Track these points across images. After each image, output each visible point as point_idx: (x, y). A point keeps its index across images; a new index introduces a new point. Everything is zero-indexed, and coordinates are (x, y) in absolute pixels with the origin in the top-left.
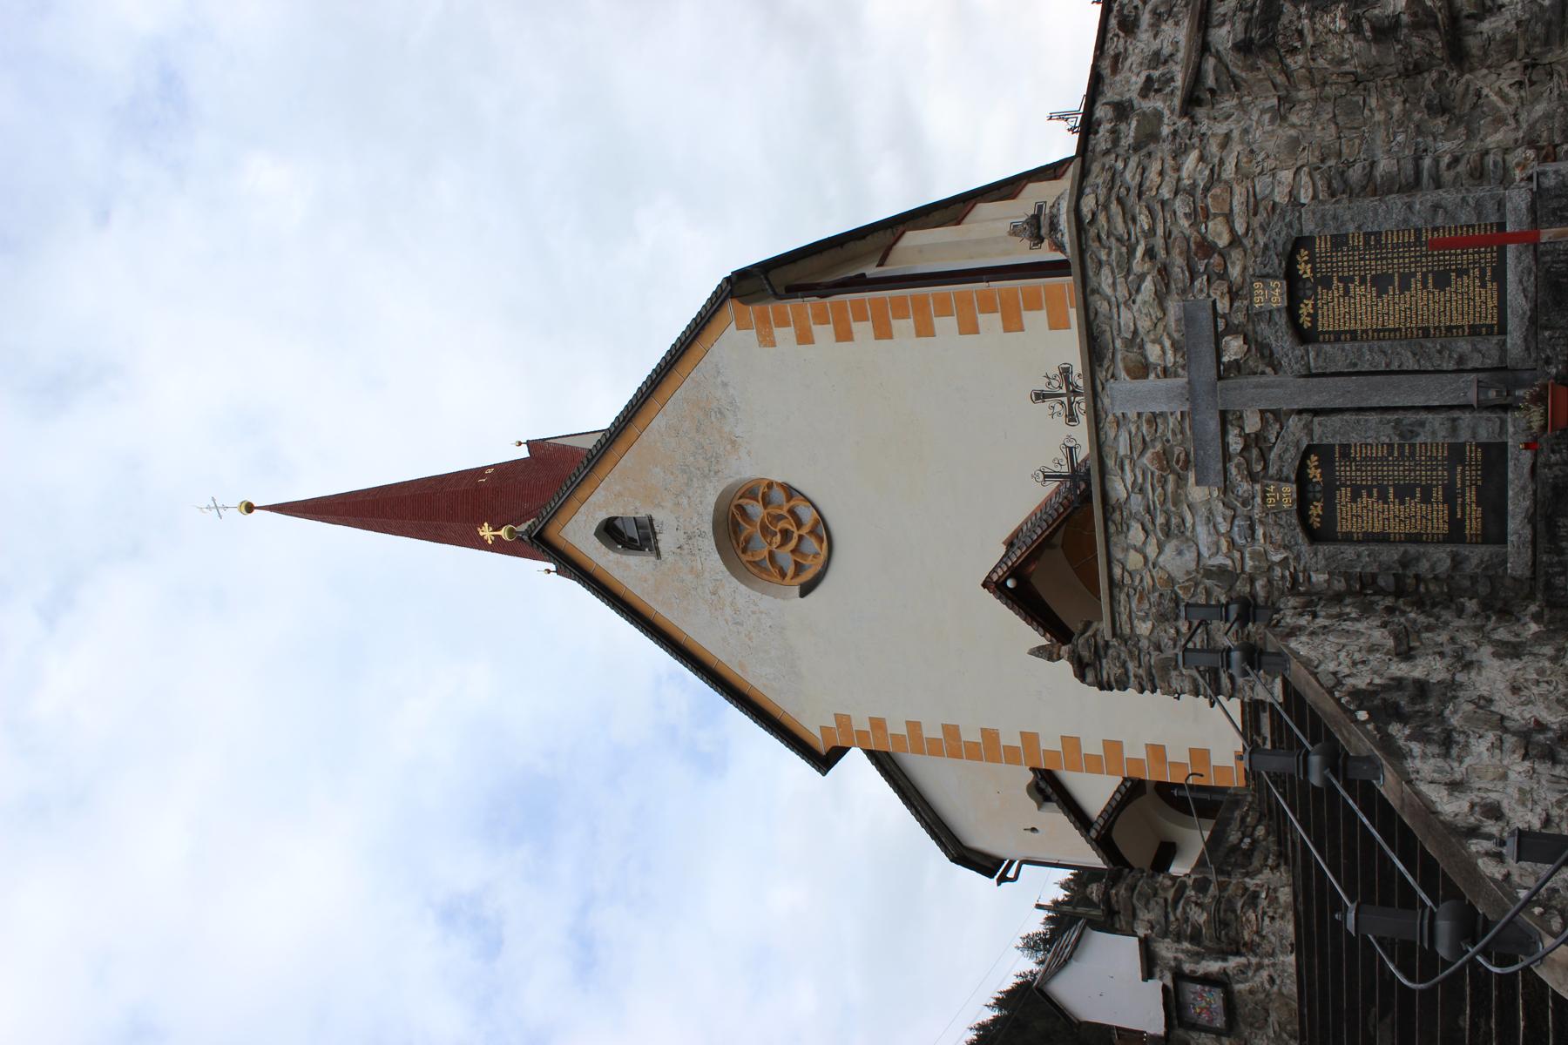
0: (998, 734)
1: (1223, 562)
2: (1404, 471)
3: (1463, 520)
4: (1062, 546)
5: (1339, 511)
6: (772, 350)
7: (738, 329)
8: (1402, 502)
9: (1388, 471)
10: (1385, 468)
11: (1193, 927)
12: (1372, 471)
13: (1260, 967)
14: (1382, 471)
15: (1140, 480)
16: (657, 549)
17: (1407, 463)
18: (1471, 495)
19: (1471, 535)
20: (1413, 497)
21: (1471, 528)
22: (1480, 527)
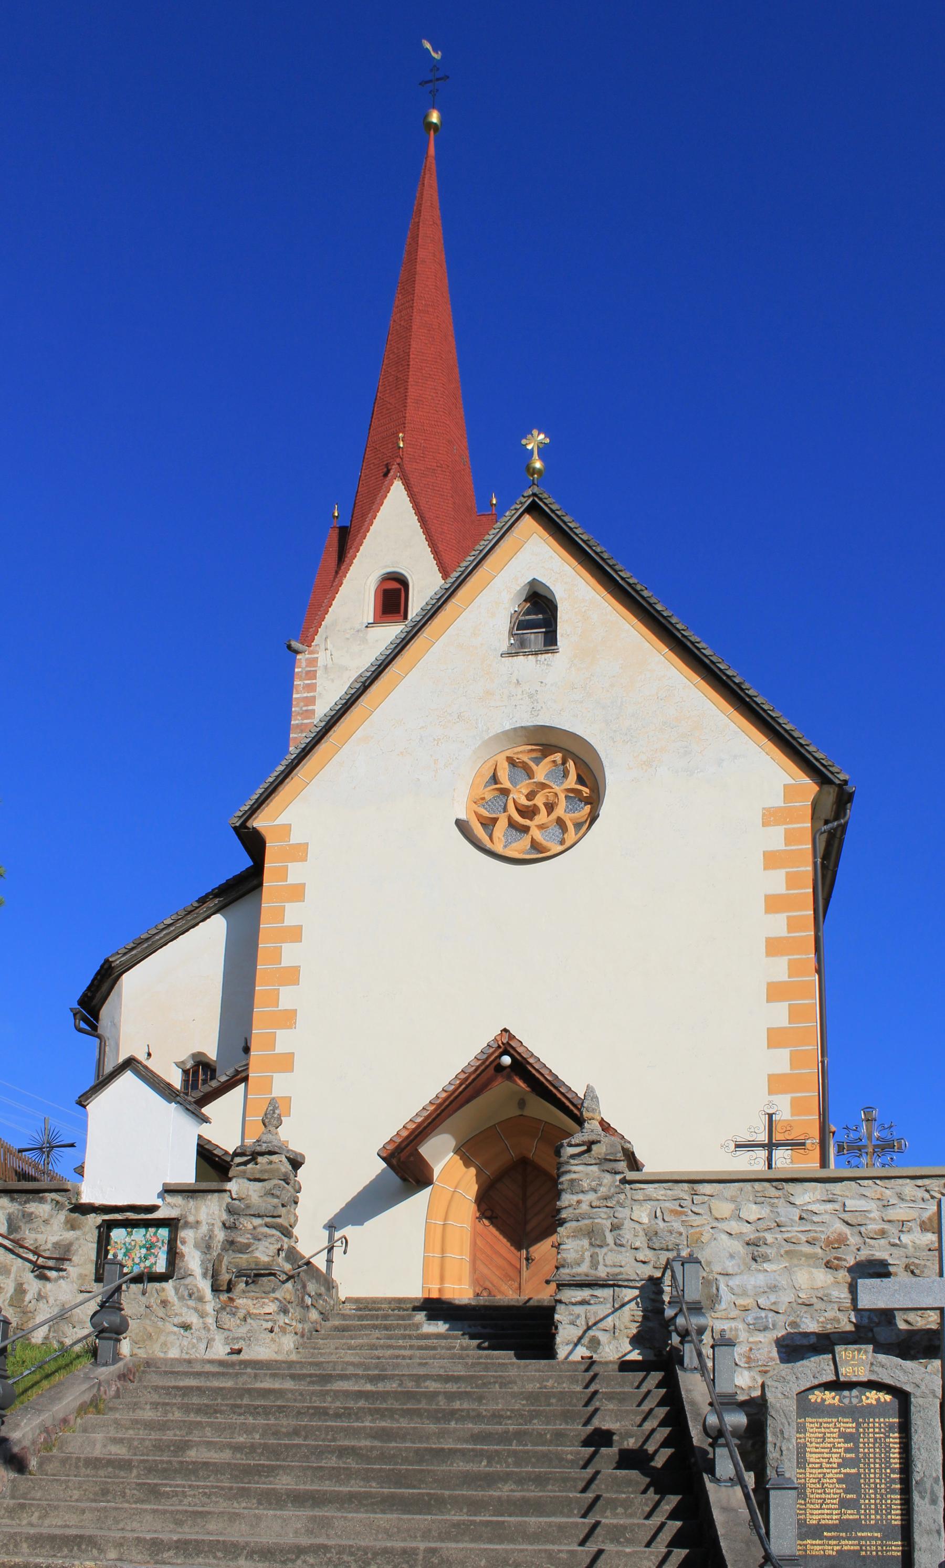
0: (290, 1027)
1: (724, 1300)
2: (876, 1484)
3: (821, 1537)
4: (521, 1115)
5: (829, 1420)
6: (759, 821)
7: (786, 786)
8: (840, 1481)
9: (875, 1468)
10: (877, 1466)
11: (248, 1246)
12: (875, 1453)
13: (202, 1315)
14: (875, 1463)
15: (815, 1219)
16: (517, 654)
17: (883, 1486)
18: (849, 1545)
19: (806, 1545)
20: (846, 1491)
21: (812, 1545)
22: (814, 1553)
